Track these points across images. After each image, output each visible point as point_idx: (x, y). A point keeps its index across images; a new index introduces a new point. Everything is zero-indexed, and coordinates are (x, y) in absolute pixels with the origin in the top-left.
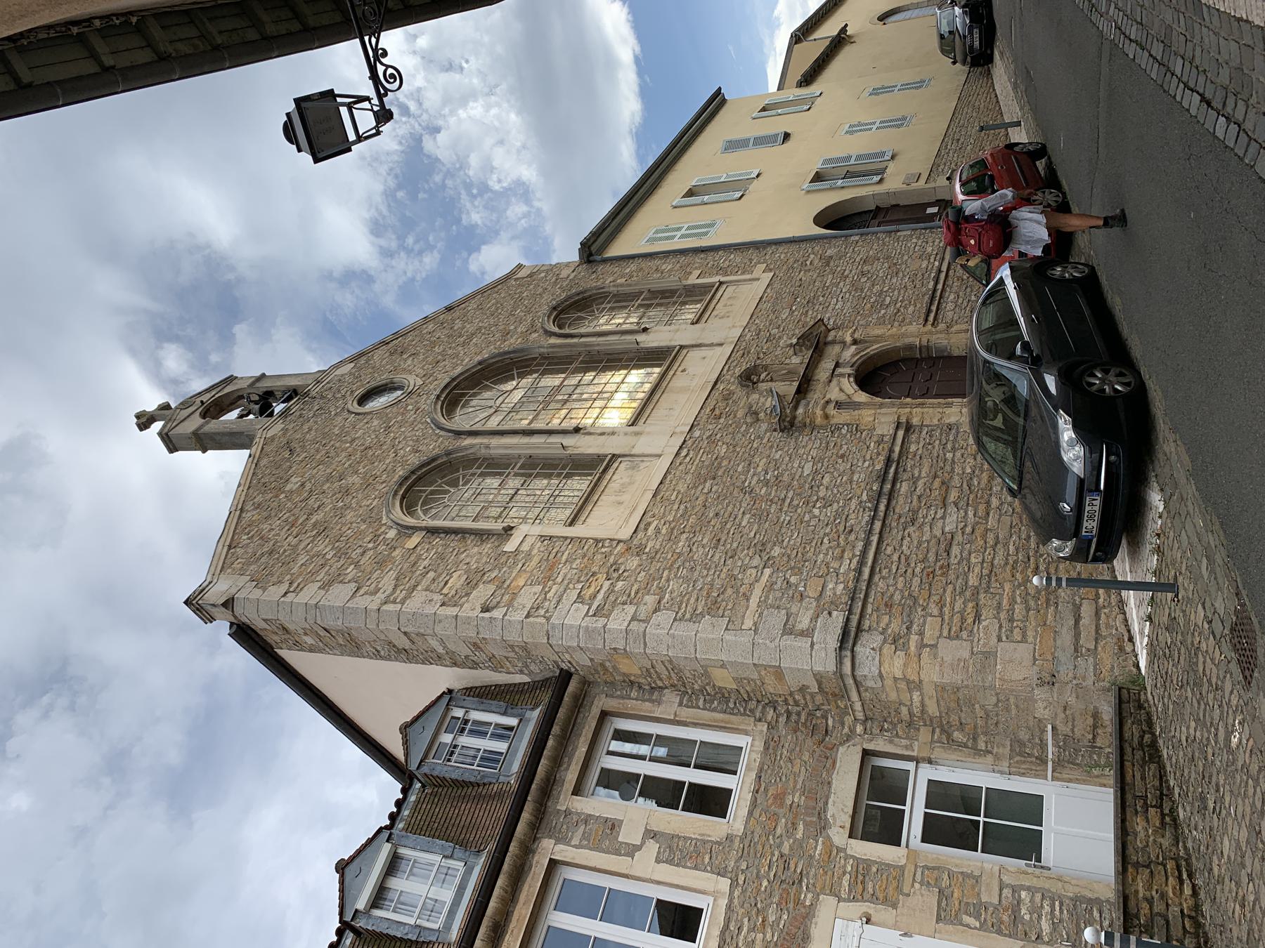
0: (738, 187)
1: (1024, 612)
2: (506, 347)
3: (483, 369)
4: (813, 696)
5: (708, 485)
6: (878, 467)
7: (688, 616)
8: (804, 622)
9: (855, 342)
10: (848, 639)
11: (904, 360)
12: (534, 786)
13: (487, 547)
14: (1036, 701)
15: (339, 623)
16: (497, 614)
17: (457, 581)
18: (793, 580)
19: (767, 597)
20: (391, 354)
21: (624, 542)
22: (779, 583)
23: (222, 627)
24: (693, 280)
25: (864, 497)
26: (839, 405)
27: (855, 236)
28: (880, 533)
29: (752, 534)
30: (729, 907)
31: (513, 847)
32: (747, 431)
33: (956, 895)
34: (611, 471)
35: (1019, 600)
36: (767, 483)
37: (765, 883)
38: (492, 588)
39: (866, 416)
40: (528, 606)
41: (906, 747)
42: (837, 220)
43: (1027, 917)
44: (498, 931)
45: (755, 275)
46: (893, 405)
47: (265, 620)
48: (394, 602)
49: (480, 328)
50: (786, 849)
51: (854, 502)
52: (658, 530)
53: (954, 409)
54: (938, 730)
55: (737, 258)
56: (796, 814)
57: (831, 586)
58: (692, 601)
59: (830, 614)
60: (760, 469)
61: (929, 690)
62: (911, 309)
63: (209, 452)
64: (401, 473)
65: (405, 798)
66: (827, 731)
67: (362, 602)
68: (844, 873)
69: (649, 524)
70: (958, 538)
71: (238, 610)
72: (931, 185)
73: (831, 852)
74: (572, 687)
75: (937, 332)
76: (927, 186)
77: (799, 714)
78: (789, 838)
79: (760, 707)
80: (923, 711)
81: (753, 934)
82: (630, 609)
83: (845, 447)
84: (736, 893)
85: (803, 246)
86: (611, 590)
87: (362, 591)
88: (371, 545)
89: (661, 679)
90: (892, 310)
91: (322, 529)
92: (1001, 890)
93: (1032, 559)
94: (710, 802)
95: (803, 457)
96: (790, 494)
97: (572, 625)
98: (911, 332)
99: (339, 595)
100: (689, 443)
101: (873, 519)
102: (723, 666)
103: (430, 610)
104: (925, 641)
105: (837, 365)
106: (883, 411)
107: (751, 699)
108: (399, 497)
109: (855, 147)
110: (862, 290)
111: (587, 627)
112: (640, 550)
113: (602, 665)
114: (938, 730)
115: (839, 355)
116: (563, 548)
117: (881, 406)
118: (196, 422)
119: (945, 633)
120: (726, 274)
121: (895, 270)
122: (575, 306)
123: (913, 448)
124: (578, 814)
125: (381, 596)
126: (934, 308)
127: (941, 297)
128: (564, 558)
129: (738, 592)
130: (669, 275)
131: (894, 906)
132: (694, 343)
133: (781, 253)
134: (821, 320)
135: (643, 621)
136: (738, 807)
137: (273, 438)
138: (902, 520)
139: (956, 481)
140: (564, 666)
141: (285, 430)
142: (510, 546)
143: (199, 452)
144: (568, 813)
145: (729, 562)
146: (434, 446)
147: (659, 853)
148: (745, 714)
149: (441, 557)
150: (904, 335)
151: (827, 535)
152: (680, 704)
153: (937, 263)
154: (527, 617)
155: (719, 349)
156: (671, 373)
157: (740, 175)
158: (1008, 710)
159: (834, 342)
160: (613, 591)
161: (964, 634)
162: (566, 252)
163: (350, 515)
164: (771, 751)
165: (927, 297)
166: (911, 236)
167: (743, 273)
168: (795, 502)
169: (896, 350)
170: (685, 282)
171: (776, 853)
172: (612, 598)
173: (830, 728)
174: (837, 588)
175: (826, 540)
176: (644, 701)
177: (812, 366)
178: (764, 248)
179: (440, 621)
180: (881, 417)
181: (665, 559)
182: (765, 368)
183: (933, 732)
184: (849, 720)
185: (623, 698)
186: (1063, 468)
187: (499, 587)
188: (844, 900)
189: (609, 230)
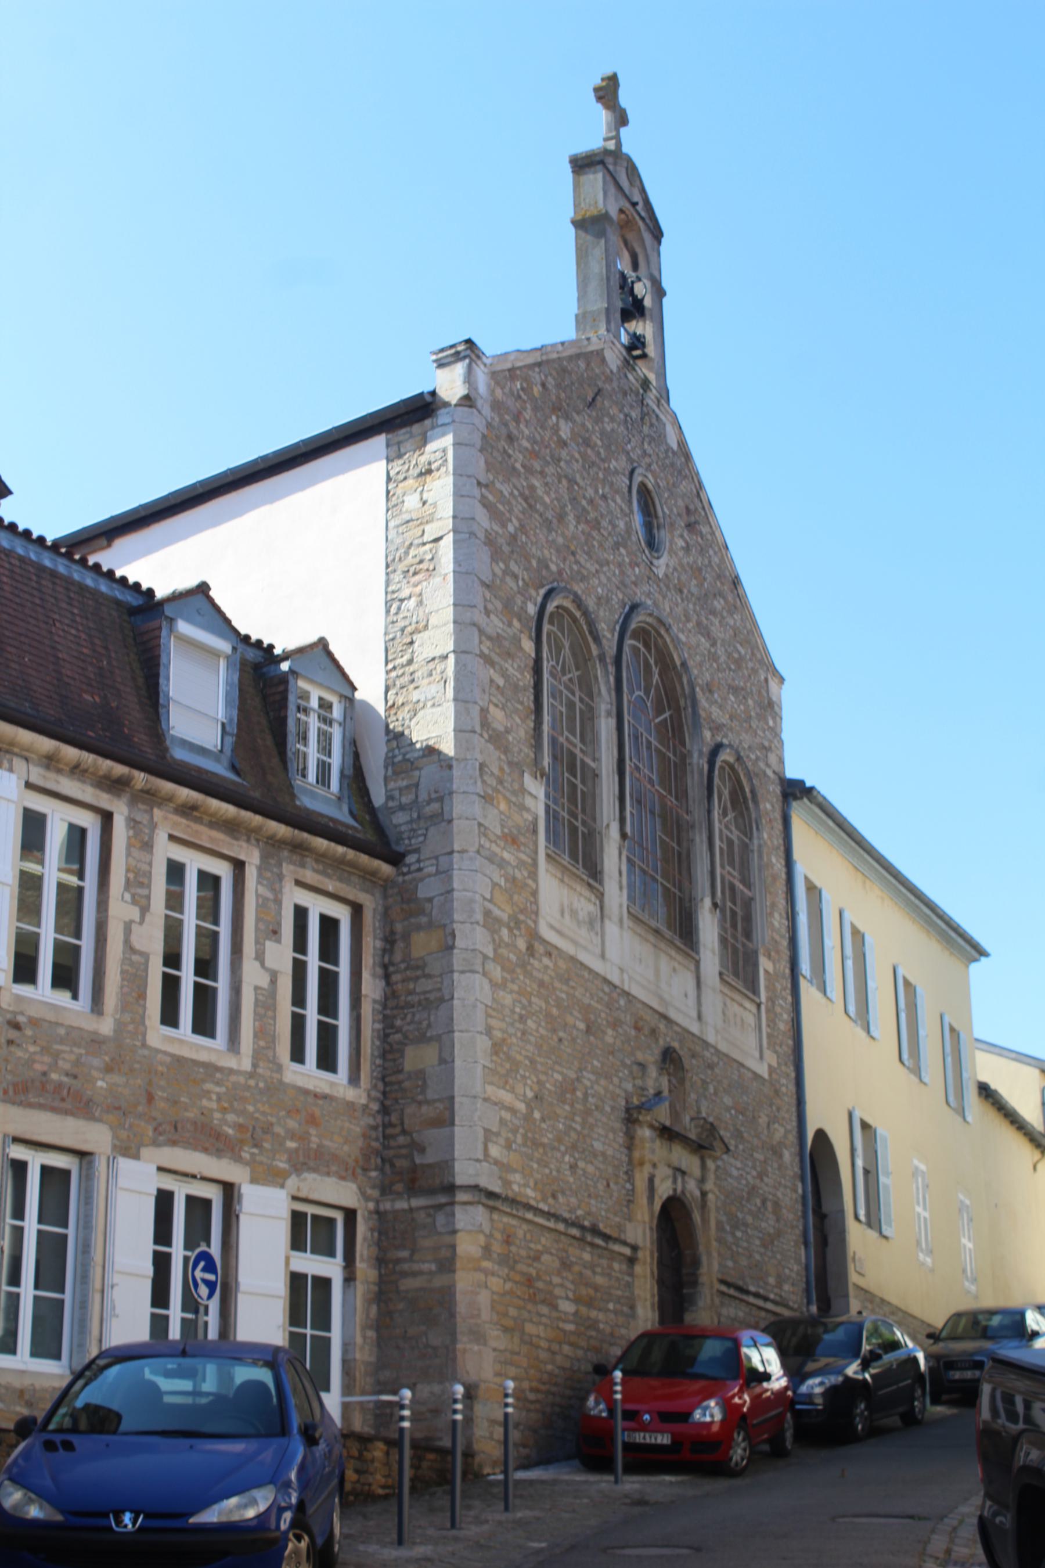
8: (495, 1151)
12: (305, 835)
13: (528, 752)
24: (765, 964)
30: (231, 1071)
40: (487, 825)
41: (362, 1255)
42: (818, 1159)
45: (767, 1053)
55: (783, 1025)
70: (555, 1314)
75: (712, 1295)
80: (404, 1274)
82: (491, 955)
89: (403, 981)
98: (712, 1267)
102: (442, 1061)
113: (421, 912)
119: (495, 1297)
120: (768, 1011)
121: (769, 1241)
132: (702, 979)
133: (788, 1087)
139: (594, 1314)
140: (411, 859)
144: (280, 877)
150: (709, 1254)
154: (480, 825)
155: (694, 1014)
165: (740, 1283)
169: (693, 1244)
170: (761, 951)
180: (641, 1231)
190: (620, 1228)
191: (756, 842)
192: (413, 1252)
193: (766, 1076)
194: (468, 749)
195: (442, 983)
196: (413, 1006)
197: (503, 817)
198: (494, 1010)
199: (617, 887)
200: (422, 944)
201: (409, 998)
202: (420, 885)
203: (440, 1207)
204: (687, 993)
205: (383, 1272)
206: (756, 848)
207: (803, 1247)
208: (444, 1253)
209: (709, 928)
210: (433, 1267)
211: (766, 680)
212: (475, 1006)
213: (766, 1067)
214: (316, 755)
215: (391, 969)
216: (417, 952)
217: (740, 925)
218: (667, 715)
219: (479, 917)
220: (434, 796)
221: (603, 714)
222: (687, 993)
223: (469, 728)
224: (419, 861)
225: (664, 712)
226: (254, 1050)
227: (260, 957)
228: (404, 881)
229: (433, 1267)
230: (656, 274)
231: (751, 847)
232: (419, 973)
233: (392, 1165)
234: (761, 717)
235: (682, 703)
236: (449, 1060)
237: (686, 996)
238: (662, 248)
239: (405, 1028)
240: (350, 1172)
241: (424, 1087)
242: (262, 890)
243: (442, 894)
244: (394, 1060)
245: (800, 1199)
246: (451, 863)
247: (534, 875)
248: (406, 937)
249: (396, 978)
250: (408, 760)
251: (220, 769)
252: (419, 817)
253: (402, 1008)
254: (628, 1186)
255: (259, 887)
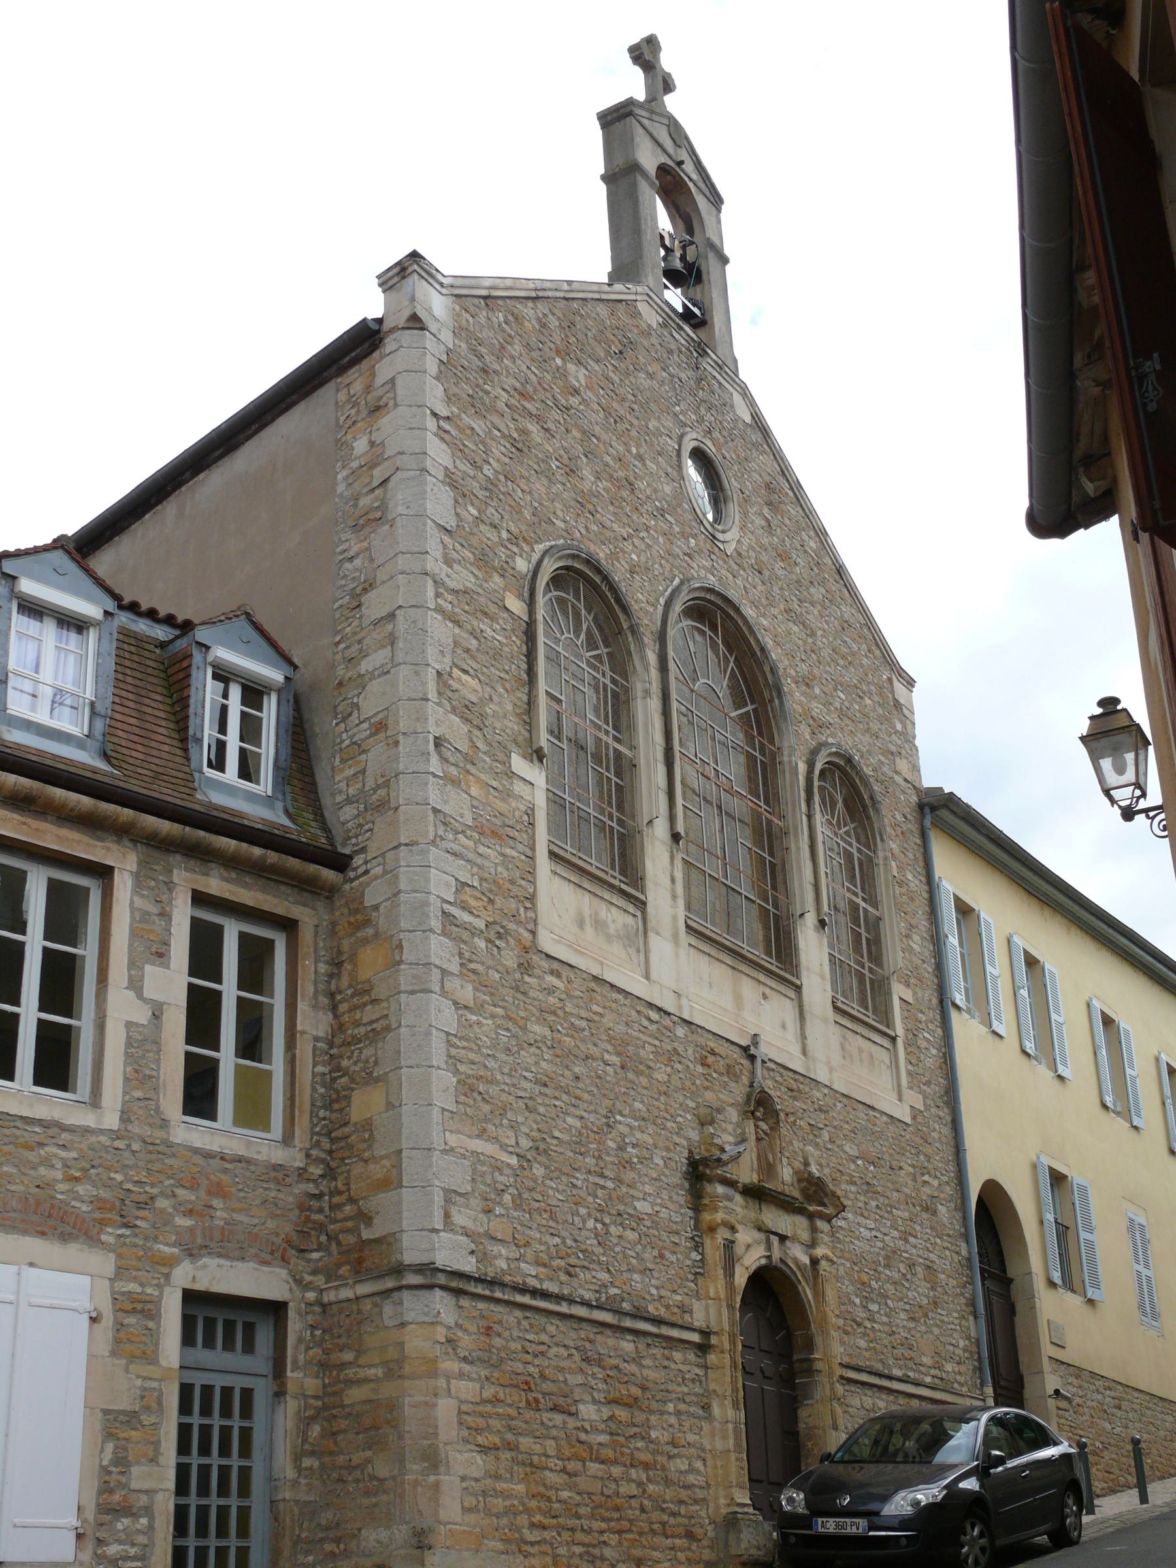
0: (1044, 1047)
1: (495, 1511)
2: (788, 685)
3: (754, 654)
4: (355, 1230)
5: (614, 1059)
6: (651, 1308)
7: (453, 1052)
8: (460, 1218)
9: (815, 1262)
10: (458, 1284)
11: (789, 1337)
12: (202, 833)
13: (513, 725)
14: (388, 1527)
15: (401, 509)
16: (435, 764)
17: (469, 688)
18: (507, 1198)
19: (483, 1163)
20: (768, 486)
21: (533, 942)
22: (501, 1179)
23: (373, 305)
24: (899, 991)
25: (613, 1291)
26: (729, 1245)
27: (969, 1249)
28: (571, 1316)
29: (557, 1134)
30: (87, 1130)
31: (127, 813)
32: (686, 1109)
33: (134, 1433)
34: (621, 902)
35: (508, 1503)
36: (621, 1148)
37: (119, 1177)
38: (464, 746)
39: (716, 1286)
40: (446, 809)
41: (295, 1361)
43: (119, 1526)
44: (21, 802)
45: (907, 1093)
46: (732, 1324)
47: (392, 381)
48: (438, 595)
49: (813, 634)
50: (162, 1203)
51: (604, 1276)
52: (551, 991)
53: (730, 1413)
54: (320, 1403)
55: (931, 1059)
56: (202, 1215)
57: (503, 1251)
58: (472, 1056)
59: (472, 1252)
60: (639, 1135)
61: (388, 1390)
62: (862, 1343)
63: (602, 188)
64: (601, 554)
65: (140, 614)
66: (303, 1251)
67: (434, 543)
68: (142, 1285)
69: (558, 975)
70: (572, 1423)
71: (407, 337)
72: (1047, 1366)
73: (164, 1265)
74: (328, 874)
75: (832, 1384)
76: (1045, 1360)
77: (320, 1210)
78: (174, 1208)
79: (323, 1155)
80: (349, 1382)
81: (59, 1166)
82: (454, 967)
83: (674, 1258)
84: (103, 1139)
85: (952, 1167)
86: (474, 932)
87: (447, 539)
88: (504, 535)
89: (350, 1011)
90: (861, 1314)
91: (519, 446)
92: (147, 1492)
93: (554, 1521)
94: (200, 1096)
95: (659, 1198)
96: (610, 1184)
97: (427, 877)
98: (835, 1348)
99: (439, 504)
100: (667, 1021)
101: (585, 1303)
102: (390, 1106)
103: (431, 655)
104: (453, 1381)
105: (783, 1238)
106: (725, 1311)
107: (333, 1141)
108: (570, 563)
109: (1105, 1241)
110: (887, 1266)
111: (427, 904)
112: (525, 967)
113: (367, 922)
114: (320, 1403)
115: (794, 1239)
116: (520, 847)
117: (731, 1307)
118: (649, 160)
119: (464, 1408)
120: (907, 1045)
122: (848, 788)
123: (677, 1355)
124: (171, 900)
125: (441, 569)
126: (864, 1377)
127: (881, 1388)
128: (508, 851)
129: (486, 1120)
130: (902, 949)
131: (113, 1353)
132: (806, 1008)
133: (940, 1132)
134: (844, 1208)
135: (442, 987)
136: (192, 1133)
137: (636, 314)
138: (587, 1345)
139: (640, 1417)
140: (358, 861)
141: (647, 332)
142: (518, 764)
143: (602, 170)
144: (170, 886)
145: (521, 1103)
146: (645, 600)
147: (137, 1025)
148: (313, 1134)
149: (497, 655)
151: (564, 1242)
152: (316, 1039)
153: (928, 1380)
154: (436, 811)
155: (796, 1049)
156: (762, 978)
157: (1062, 1046)
158: (367, 1494)
159: (814, 1230)
160: (473, 934)
161: (465, 1433)
162: (936, 773)
163: (540, 486)
164: (272, 1174)
165: (879, 1367)
166: (968, 1338)
167: (909, 1073)
168: (600, 1193)
169: (805, 1322)
171: (155, 1191)
172: (465, 935)
173: (307, 1255)
174: (501, 1260)
175: (557, 1240)
176: (315, 982)
177: (786, 1204)
178: (947, 1103)
179: (417, 673)
180: (714, 1309)
181: (518, 1007)
182: (775, 1127)
183: (316, 1397)
184: (320, 1280)
185: (315, 951)
186: (885, 1498)
187: (466, 757)
188: (112, 1287)
189: (973, 834)
190: (684, 1309)
191: (880, 854)
192: (359, 1353)
193: (908, 1120)
194: (418, 719)
195: (388, 1008)
196: (360, 1042)
197: (475, 803)
198: (461, 1038)
199: (668, 895)
200: (369, 963)
201: (356, 1031)
202: (367, 890)
203: (387, 1293)
204: (796, 1028)
205: (327, 1381)
206: (881, 861)
207: (971, 1318)
208: (392, 1354)
209: (813, 950)
210: (379, 1372)
211: (890, 680)
212: (428, 1034)
213: (908, 1110)
214: (263, 751)
215: (338, 997)
216: (364, 974)
217: (864, 942)
218: (750, 707)
219: (435, 923)
220: (380, 781)
221: (639, 694)
222: (796, 1028)
223: (421, 695)
224: (366, 862)
225: (746, 705)
226: (124, 1103)
227: (135, 985)
228: (352, 889)
229: (379, 1372)
230: (715, 239)
231: (876, 861)
232: (366, 998)
233: (339, 1243)
234: (886, 719)
235: (767, 695)
236: (397, 1105)
237: (784, 1027)
238: (722, 215)
239: (353, 1068)
240: (278, 1255)
241: (370, 1141)
242: (139, 902)
243: (389, 899)
244: (341, 1110)
245: (964, 1262)
246: (397, 860)
247: (531, 874)
248: (353, 957)
249: (343, 1007)
250: (355, 743)
251: (86, 758)
252: (366, 809)
253: (349, 1044)
254: (695, 1256)
255: (135, 898)
